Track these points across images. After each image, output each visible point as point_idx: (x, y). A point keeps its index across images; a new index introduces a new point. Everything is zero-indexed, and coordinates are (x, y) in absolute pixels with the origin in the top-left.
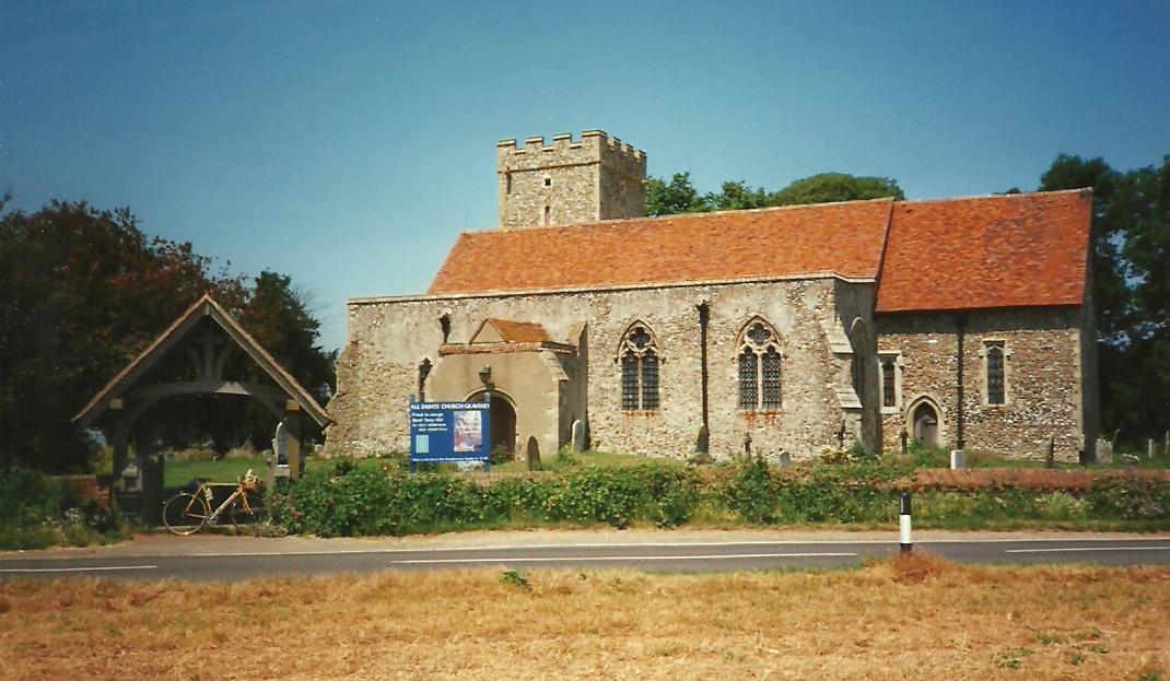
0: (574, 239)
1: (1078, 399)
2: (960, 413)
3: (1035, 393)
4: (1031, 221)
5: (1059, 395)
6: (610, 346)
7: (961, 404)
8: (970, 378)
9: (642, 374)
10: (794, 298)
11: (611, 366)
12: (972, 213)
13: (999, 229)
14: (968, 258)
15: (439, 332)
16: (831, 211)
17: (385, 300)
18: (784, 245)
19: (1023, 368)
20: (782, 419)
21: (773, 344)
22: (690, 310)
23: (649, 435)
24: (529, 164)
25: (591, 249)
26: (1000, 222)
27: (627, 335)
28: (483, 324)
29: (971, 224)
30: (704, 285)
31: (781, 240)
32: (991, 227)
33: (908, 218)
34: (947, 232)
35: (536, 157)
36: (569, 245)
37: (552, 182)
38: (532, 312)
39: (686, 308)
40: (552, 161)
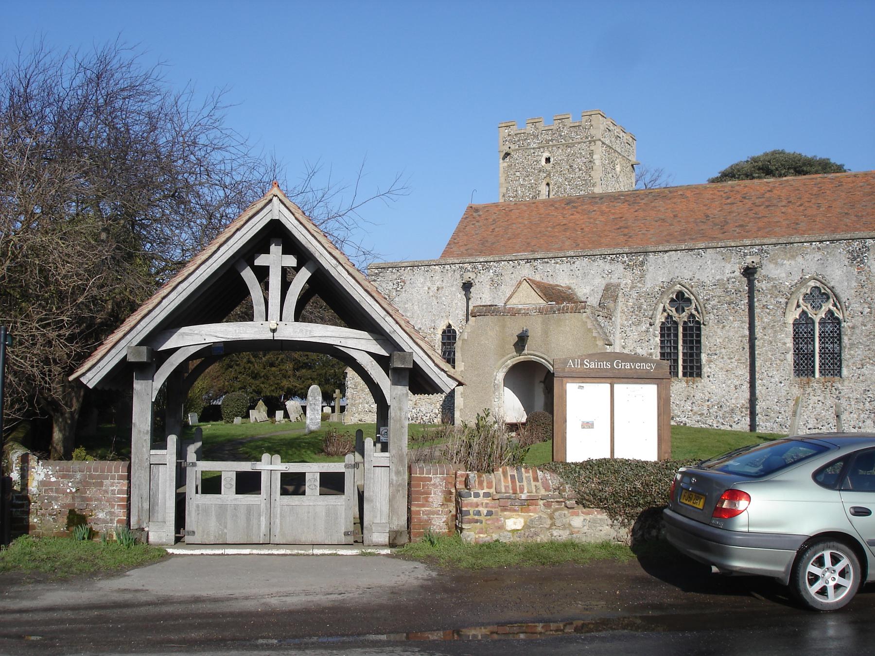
0: (584, 210)
15: (461, 295)
17: (406, 264)
18: (806, 212)
20: (840, 387)
22: (737, 273)
23: (689, 403)
24: (529, 144)
28: (520, 283)
30: (752, 246)
31: (802, 208)
36: (577, 216)
37: (552, 160)
39: (732, 269)
40: (552, 140)
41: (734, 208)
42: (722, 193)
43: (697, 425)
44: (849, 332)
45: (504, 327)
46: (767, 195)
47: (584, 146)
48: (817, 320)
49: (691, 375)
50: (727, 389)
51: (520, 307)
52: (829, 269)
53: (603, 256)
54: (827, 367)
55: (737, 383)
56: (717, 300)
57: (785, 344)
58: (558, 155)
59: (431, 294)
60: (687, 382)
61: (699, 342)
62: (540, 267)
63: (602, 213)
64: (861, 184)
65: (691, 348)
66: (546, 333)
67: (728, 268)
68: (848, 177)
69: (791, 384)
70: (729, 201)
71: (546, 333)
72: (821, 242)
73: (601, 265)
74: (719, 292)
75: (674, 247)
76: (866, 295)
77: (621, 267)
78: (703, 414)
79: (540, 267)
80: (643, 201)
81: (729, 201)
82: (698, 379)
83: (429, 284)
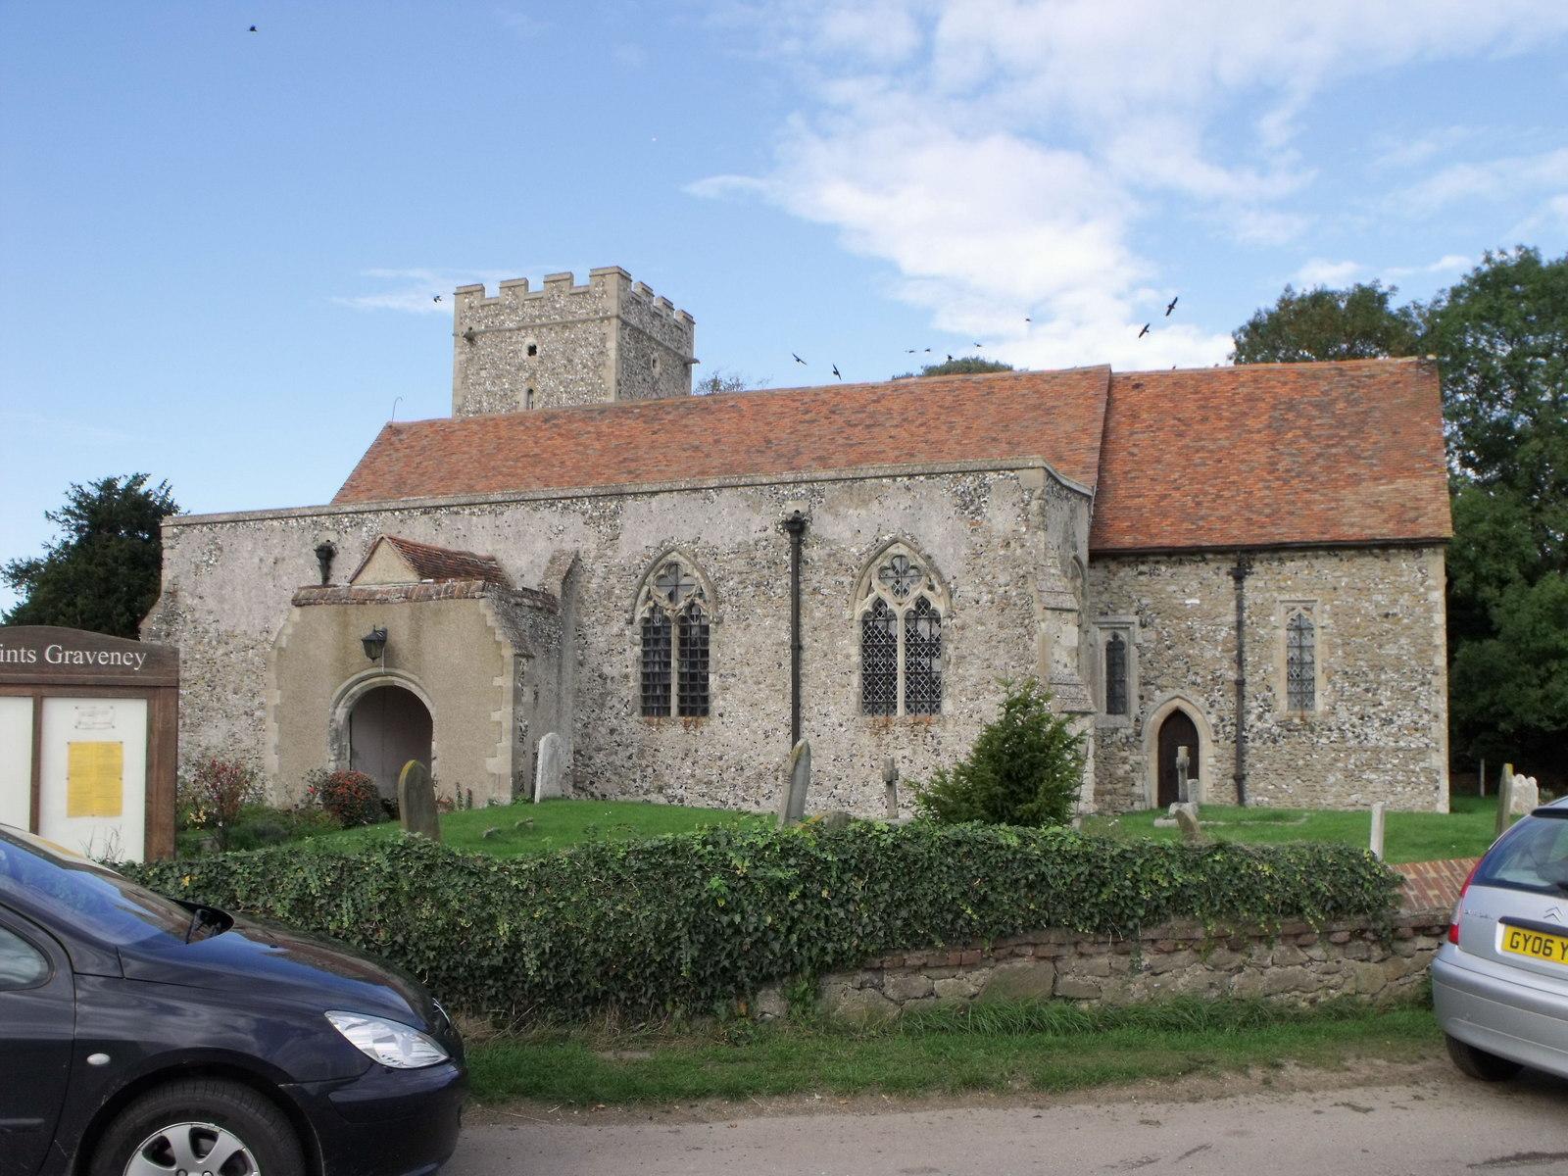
1: (1441, 704)
2: (1240, 725)
3: (1367, 690)
4: (1341, 405)
5: (1407, 695)
6: (619, 598)
7: (1241, 713)
8: (1257, 666)
9: (678, 669)
10: (969, 505)
11: (621, 635)
12: (1243, 390)
13: (1290, 416)
14: (1243, 461)
16: (1007, 384)
18: (930, 436)
19: (1348, 648)
21: (927, 594)
22: (771, 532)
24: (503, 322)
25: (597, 445)
26: (1291, 406)
27: (651, 578)
29: (1244, 407)
30: (796, 483)
31: (923, 429)
32: (1277, 414)
33: (1135, 397)
34: (1204, 420)
35: (514, 310)
36: (559, 441)
38: (476, 535)
40: (540, 317)
41: (816, 431)
42: (798, 404)
43: (701, 803)
44: (956, 636)
45: (345, 625)
46: (871, 408)
47: (591, 326)
48: (900, 612)
49: (693, 713)
50: (752, 737)
51: (375, 588)
52: (922, 525)
53: (551, 502)
54: (919, 698)
55: (769, 727)
56: (737, 579)
57: (848, 657)
58: (547, 342)
59: (265, 570)
60: (686, 726)
61: (706, 653)
62: (446, 521)
63: (599, 435)
64: (1025, 391)
65: (693, 665)
66: (416, 634)
67: (757, 522)
68: (1003, 379)
69: (858, 729)
70: (807, 417)
71: (416, 634)
72: (911, 476)
73: (549, 516)
74: (740, 564)
75: (668, 486)
76: (987, 570)
77: (580, 520)
78: (709, 783)
79: (446, 521)
80: (670, 417)
81: (807, 417)
82: (703, 719)
83: (261, 553)
